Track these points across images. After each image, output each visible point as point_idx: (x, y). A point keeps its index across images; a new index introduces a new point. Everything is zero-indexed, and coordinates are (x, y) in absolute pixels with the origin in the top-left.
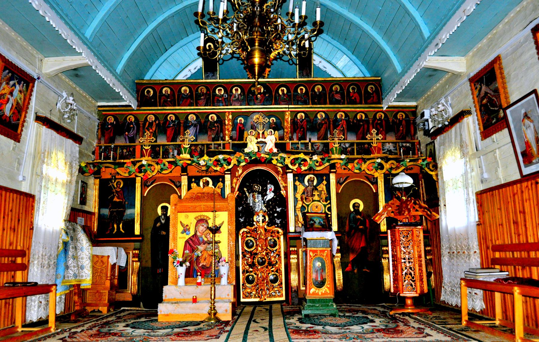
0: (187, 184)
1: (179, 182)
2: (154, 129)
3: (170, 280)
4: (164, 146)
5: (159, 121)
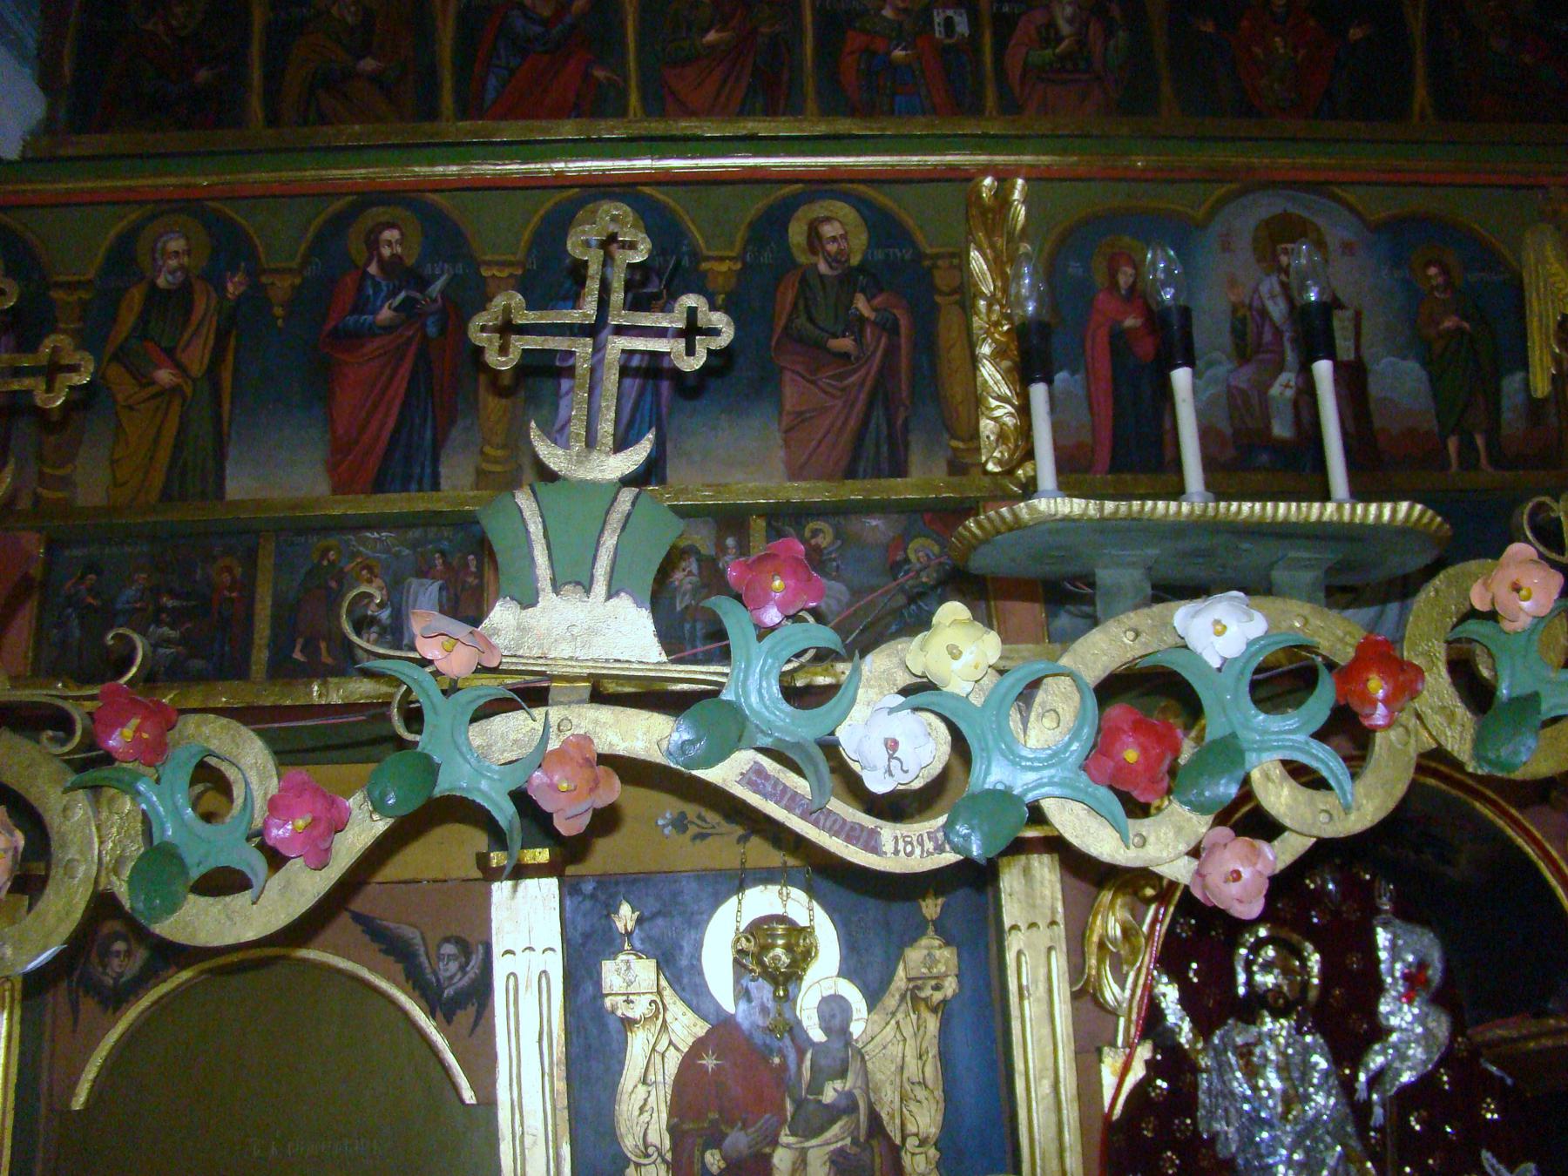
0: (555, 966)
1: (465, 948)
2: (197, 357)
3: (18, 986)
4: (300, 528)
5: (254, 273)
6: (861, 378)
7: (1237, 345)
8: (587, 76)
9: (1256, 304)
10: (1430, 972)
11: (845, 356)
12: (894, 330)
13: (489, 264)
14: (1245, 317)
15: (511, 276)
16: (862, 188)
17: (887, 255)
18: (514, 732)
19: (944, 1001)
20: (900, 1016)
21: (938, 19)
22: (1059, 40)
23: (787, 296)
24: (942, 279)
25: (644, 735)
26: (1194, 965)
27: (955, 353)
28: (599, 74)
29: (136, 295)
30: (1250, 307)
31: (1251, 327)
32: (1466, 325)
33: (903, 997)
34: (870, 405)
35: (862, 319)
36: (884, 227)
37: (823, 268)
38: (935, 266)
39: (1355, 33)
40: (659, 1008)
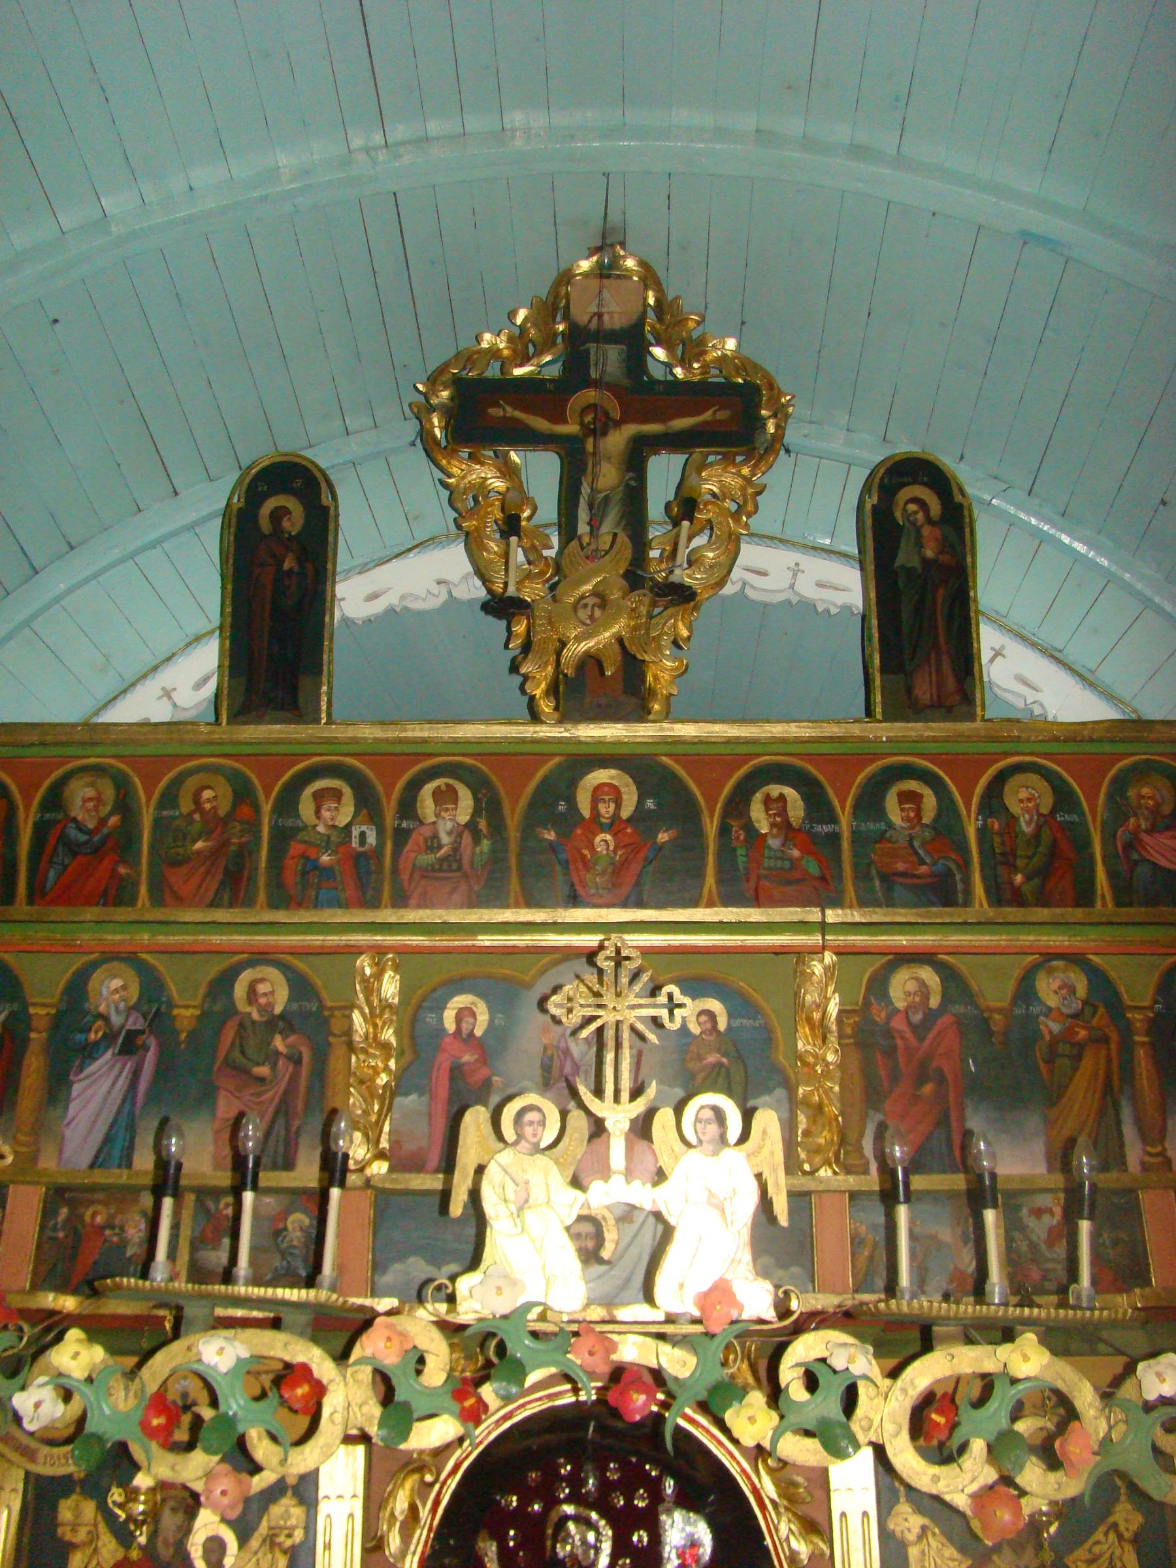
6: (272, 1095)
7: (544, 1077)
8: (114, 870)
9: (562, 1044)
10: (701, 1550)
11: (261, 1080)
12: (298, 1062)
13: (35, 1005)
14: (552, 1055)
15: (48, 1014)
16: (288, 957)
17: (300, 1007)
19: (293, 1547)
20: (260, 1555)
21: (355, 832)
22: (440, 847)
23: (229, 1033)
24: (337, 1026)
26: (512, 1533)
27: (340, 1078)
28: (122, 870)
30: (557, 1048)
31: (556, 1064)
32: (725, 1060)
33: (264, 1541)
34: (277, 1113)
35: (277, 1053)
36: (300, 986)
37: (256, 1016)
38: (332, 1016)
39: (663, 837)
40: (94, 1536)
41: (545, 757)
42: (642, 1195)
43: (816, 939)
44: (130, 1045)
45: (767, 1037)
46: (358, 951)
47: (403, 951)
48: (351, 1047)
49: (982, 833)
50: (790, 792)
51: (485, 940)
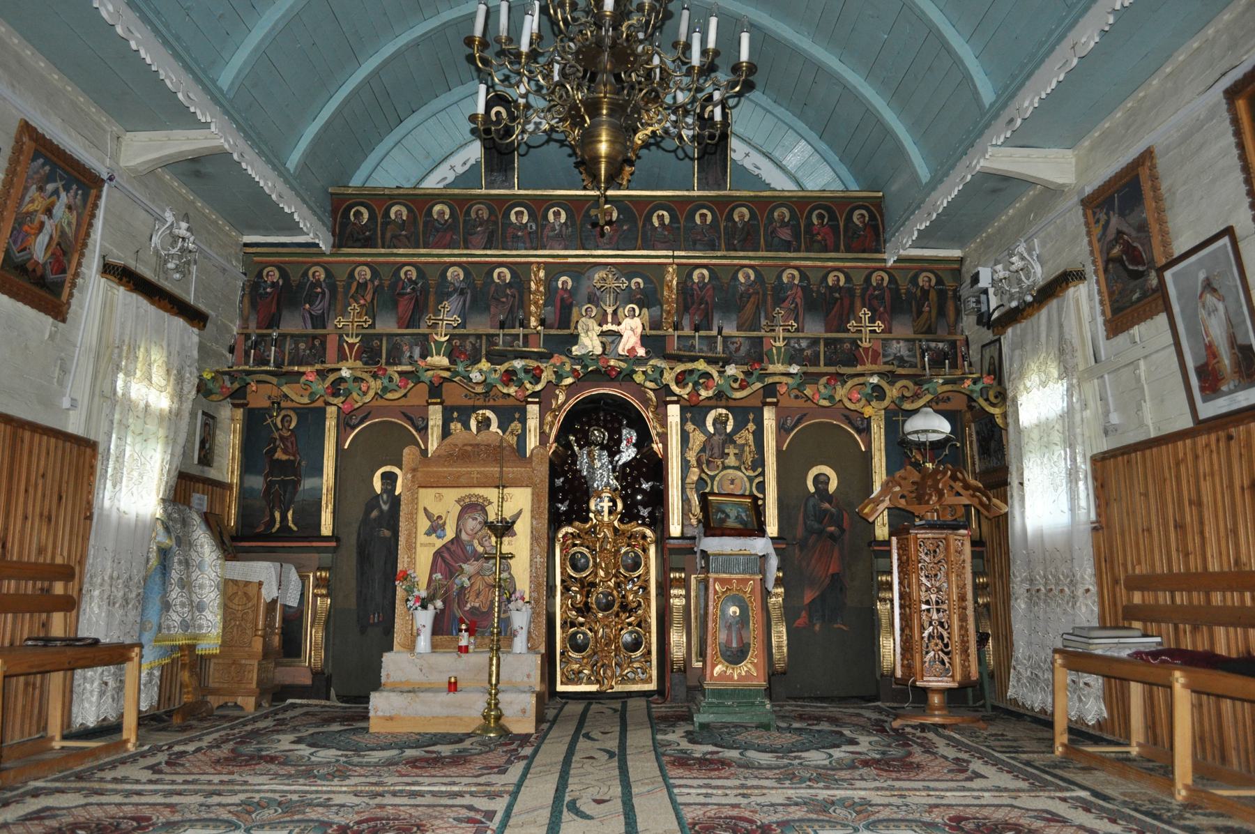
0: (440, 423)
2: (369, 298)
5: (381, 279)
6: (507, 307)
18: (430, 373)
25: (446, 374)
29: (355, 284)
41: (588, 201)
42: (614, 328)
43: (670, 260)
44: (462, 292)
45: (655, 291)
46: (532, 263)
47: (545, 263)
48: (530, 292)
49: (725, 227)
50: (665, 213)
51: (570, 260)
